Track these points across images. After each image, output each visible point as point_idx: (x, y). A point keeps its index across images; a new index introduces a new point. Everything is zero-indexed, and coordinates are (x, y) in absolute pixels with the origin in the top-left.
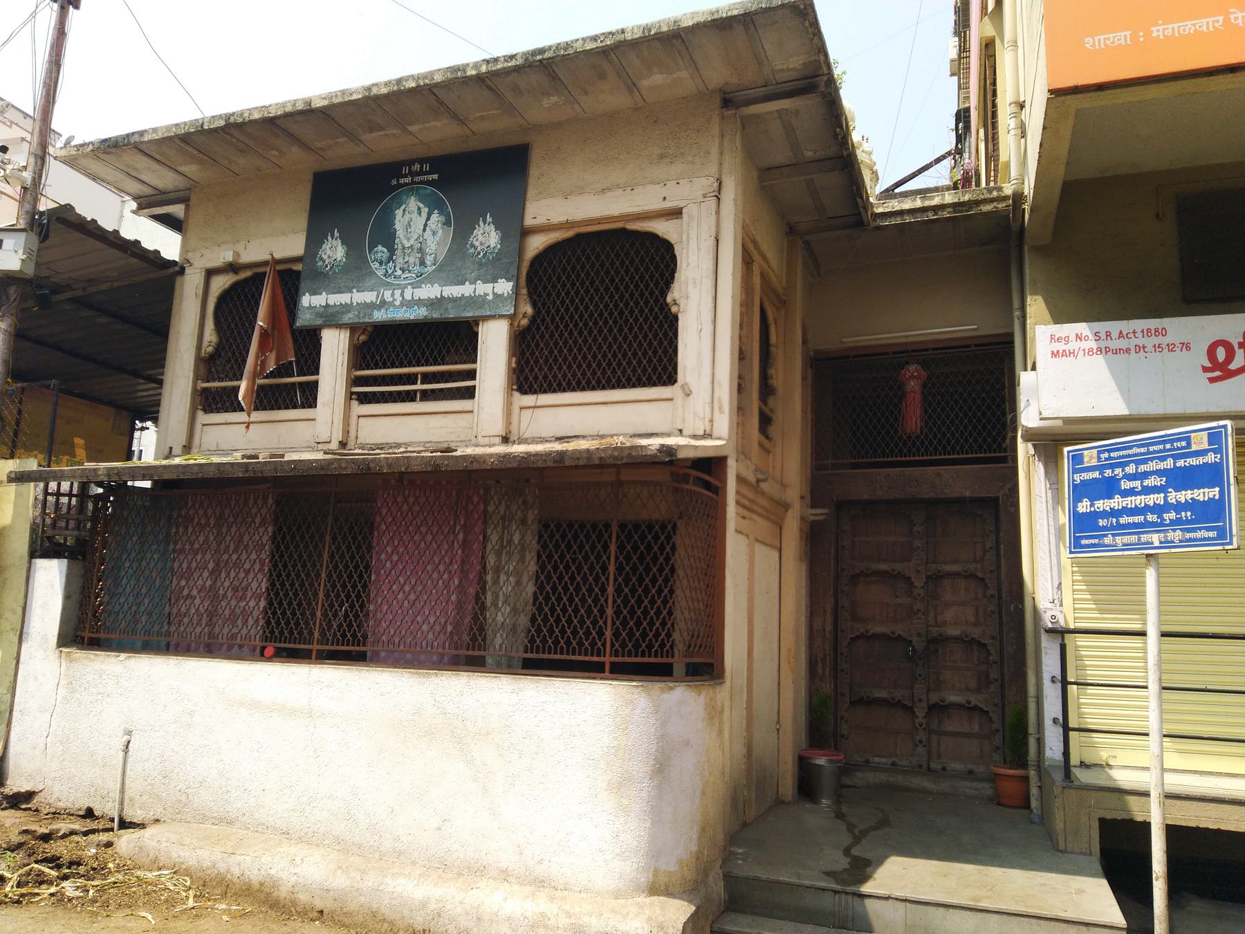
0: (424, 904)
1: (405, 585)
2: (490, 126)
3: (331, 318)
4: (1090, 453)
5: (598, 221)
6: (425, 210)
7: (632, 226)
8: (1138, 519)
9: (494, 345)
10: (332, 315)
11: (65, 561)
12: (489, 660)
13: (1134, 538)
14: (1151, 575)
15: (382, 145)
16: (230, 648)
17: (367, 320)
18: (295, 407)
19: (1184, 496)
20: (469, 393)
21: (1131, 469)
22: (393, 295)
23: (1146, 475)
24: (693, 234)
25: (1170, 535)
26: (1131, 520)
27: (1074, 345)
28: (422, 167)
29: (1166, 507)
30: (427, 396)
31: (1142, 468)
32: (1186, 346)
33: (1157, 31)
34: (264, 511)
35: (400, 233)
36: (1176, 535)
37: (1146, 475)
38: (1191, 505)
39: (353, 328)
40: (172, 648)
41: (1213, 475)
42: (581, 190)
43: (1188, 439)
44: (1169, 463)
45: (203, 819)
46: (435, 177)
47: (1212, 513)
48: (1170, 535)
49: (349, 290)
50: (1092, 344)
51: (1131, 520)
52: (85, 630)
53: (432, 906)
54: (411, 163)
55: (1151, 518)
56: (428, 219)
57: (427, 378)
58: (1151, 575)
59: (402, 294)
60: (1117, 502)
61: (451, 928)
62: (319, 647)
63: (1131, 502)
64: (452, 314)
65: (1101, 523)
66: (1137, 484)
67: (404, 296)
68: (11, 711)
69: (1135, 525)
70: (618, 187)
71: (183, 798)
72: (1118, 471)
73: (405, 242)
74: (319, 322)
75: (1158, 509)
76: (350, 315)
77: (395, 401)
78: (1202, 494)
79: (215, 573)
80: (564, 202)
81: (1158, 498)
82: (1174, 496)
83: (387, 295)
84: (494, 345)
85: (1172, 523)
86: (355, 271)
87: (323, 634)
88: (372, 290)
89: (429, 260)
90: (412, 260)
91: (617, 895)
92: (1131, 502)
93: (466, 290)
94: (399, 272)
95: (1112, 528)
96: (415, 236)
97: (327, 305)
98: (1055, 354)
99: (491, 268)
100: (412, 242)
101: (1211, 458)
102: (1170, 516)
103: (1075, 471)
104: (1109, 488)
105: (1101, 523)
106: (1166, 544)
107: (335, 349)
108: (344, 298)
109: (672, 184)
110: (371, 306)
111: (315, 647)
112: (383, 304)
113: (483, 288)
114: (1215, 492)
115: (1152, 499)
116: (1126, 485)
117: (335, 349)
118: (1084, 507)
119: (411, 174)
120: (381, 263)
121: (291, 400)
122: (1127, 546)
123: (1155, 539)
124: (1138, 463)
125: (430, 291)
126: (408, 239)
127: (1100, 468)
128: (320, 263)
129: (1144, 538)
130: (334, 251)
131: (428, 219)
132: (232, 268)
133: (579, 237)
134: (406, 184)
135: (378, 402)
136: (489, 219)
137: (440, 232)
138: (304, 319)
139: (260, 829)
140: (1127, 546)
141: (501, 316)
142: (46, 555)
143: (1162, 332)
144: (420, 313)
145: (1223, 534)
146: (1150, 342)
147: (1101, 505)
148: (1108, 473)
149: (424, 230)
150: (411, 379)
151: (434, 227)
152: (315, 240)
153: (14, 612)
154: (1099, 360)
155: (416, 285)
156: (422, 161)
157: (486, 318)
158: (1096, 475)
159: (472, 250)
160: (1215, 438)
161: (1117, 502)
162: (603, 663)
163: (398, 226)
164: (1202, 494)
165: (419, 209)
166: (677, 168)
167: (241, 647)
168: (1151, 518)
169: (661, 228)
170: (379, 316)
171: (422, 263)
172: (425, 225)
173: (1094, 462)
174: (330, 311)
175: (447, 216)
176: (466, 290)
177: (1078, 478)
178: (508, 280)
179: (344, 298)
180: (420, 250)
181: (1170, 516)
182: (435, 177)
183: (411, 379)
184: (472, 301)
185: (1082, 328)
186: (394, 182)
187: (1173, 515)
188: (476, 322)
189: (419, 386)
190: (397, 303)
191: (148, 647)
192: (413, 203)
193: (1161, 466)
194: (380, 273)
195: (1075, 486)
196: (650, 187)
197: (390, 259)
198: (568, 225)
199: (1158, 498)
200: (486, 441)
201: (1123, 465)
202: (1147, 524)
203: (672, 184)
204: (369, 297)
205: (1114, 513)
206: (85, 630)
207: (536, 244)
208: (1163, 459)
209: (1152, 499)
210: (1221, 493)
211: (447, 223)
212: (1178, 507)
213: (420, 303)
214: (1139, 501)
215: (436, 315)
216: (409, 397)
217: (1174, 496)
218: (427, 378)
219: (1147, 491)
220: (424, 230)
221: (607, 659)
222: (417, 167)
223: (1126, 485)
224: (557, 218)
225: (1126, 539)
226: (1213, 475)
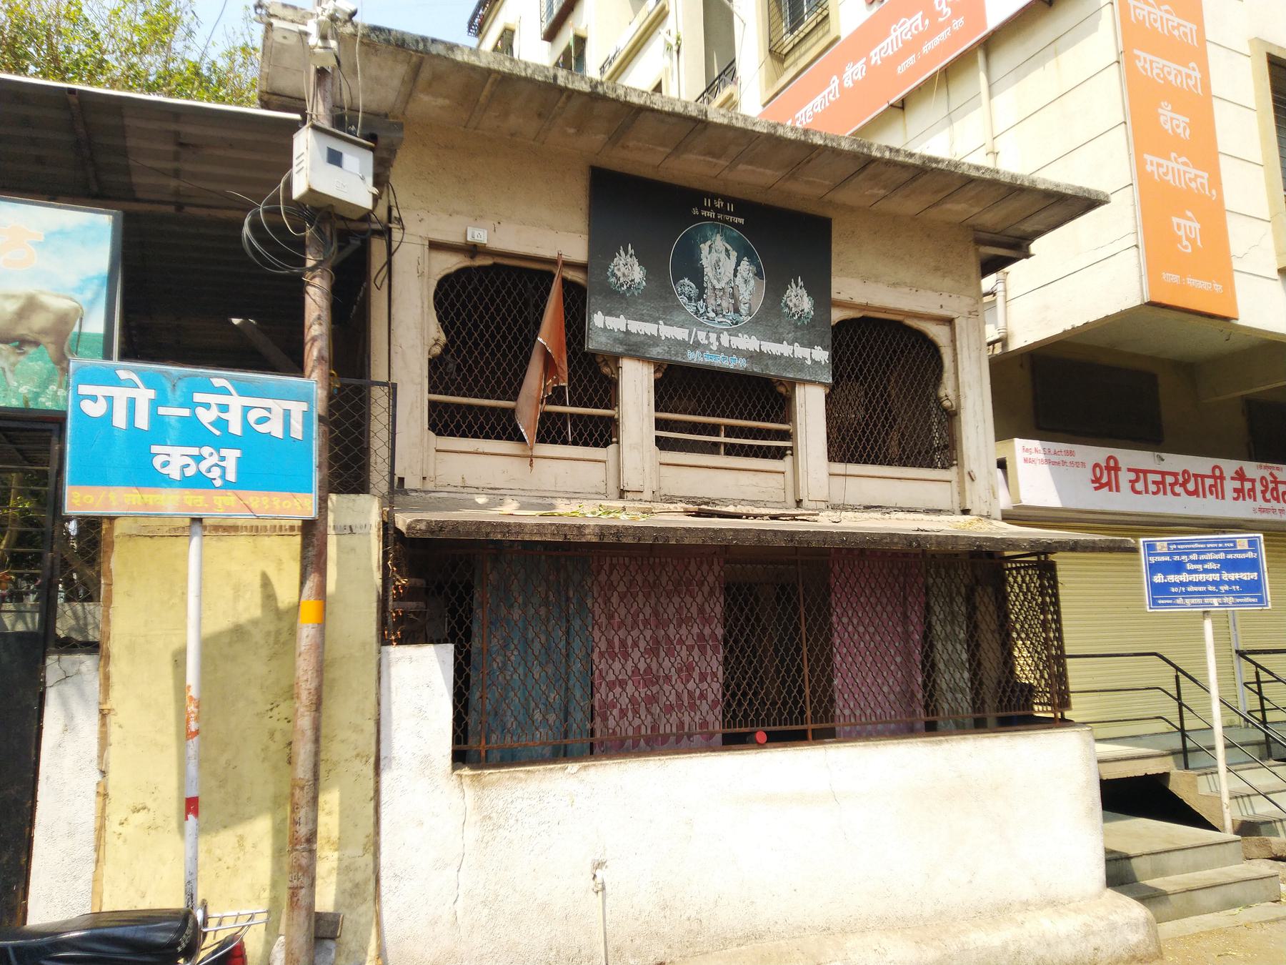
0: (1005, 948)
1: (861, 654)
2: (802, 193)
3: (636, 349)
4: (1162, 543)
5: (885, 310)
6: (734, 254)
7: (909, 322)
8: (1191, 589)
9: (811, 408)
10: (635, 344)
11: (451, 647)
12: (941, 723)
13: (1199, 601)
14: (1208, 625)
15: (690, 168)
16: (678, 740)
17: (679, 359)
18: (565, 442)
19: (1234, 576)
20: (779, 454)
21: (1194, 557)
22: (708, 338)
23: (1205, 562)
24: (965, 345)
25: (1226, 600)
26: (1196, 589)
27: (1034, 456)
28: (725, 206)
29: (1222, 582)
30: (732, 450)
31: (1202, 557)
32: (1083, 464)
33: (1191, 281)
34: (711, 579)
35: (708, 270)
36: (1230, 600)
37: (1205, 562)
38: (1239, 582)
39: (658, 365)
40: (596, 750)
41: (1253, 565)
42: (877, 279)
43: (1234, 542)
44: (1222, 556)
45: (725, 942)
46: (742, 221)
47: (1254, 588)
48: (1226, 600)
49: (655, 321)
50: (1042, 456)
51: (1196, 589)
52: (479, 742)
53: (1012, 948)
54: (714, 197)
55: (1210, 588)
56: (738, 264)
57: (731, 431)
58: (1208, 625)
59: (718, 339)
60: (1184, 577)
61: (1030, 960)
62: (814, 726)
63: (1195, 578)
64: (772, 372)
65: (1173, 590)
66: (1199, 567)
67: (725, 344)
68: (377, 881)
69: (1199, 593)
70: (905, 284)
71: (695, 926)
72: (1184, 558)
73: (715, 282)
74: (619, 349)
75: (1214, 583)
76: (659, 349)
77: (765, 456)
78: (1246, 576)
79: (653, 651)
80: (863, 285)
81: (1216, 577)
82: (1226, 576)
83: (702, 336)
84: (811, 408)
85: (1226, 592)
86: (658, 299)
87: (815, 713)
88: (682, 326)
89: (744, 309)
90: (725, 304)
91: (1099, 896)
92: (1195, 578)
93: (783, 349)
94: (712, 315)
95: (1182, 593)
96: (726, 280)
97: (628, 332)
98: (1026, 460)
99: (807, 332)
100: (722, 285)
101: (1250, 555)
102: (1225, 588)
103: (1150, 555)
104: (1178, 568)
105: (1173, 590)
106: (1222, 604)
107: (636, 385)
108: (648, 328)
109: (945, 295)
110: (683, 344)
111: (810, 726)
112: (697, 345)
113: (801, 352)
114: (1254, 575)
115: (1211, 577)
116: (1190, 566)
117: (636, 385)
118: (1159, 578)
119: (713, 207)
120: (690, 299)
121: (559, 433)
122: (1193, 605)
123: (1215, 601)
124: (1199, 553)
125: (748, 343)
126: (718, 281)
127: (1171, 555)
128: (613, 280)
129: (1207, 601)
130: (628, 269)
131: (738, 264)
132: (473, 250)
133: (864, 319)
134: (708, 219)
135: (757, 456)
136: (801, 283)
137: (752, 282)
138: (595, 343)
139: (796, 934)
140: (1193, 605)
141: (821, 383)
142: (410, 637)
143: (1071, 453)
144: (738, 364)
145: (1261, 600)
146: (1068, 459)
147: (1172, 578)
148: (1176, 558)
149: (735, 276)
150: (714, 430)
151: (745, 275)
152: (602, 248)
153: (358, 729)
154: (1046, 467)
155: (733, 333)
156: (726, 199)
157: (804, 382)
158: (1168, 559)
159: (786, 310)
160: (1252, 543)
161: (1184, 577)
162: (805, 731)
163: (704, 262)
164: (1246, 576)
165: (727, 250)
166: (948, 282)
167: (690, 736)
168: (1210, 588)
169: (938, 333)
170: (694, 357)
171: (737, 311)
172: (736, 271)
173: (1165, 550)
174: (633, 339)
175: (758, 266)
176: (783, 349)
177: (1153, 560)
178: (824, 349)
179: (648, 328)
180: (733, 296)
181: (1225, 588)
182: (742, 221)
183: (714, 430)
184: (791, 362)
185: (1036, 444)
186: (695, 212)
187: (1227, 588)
188: (792, 384)
189: (722, 439)
190: (714, 348)
191: (561, 753)
192: (719, 242)
193: (1217, 557)
194: (690, 309)
195: (1151, 565)
196: (929, 293)
197: (700, 297)
198: (866, 307)
199: (1216, 577)
200: (813, 505)
201: (1188, 554)
202: (1208, 592)
203: (945, 295)
204: (680, 334)
205: (1182, 584)
206: (479, 742)
207: (837, 315)
208: (1217, 552)
209: (1211, 577)
210: (1259, 576)
211: (758, 274)
212: (1230, 583)
213: (738, 352)
214: (1203, 577)
215: (757, 369)
216: (713, 449)
217: (1226, 576)
218: (731, 431)
219: (1206, 571)
220: (735, 276)
221: (810, 726)
222: (719, 204)
223: (1190, 566)
224: (860, 299)
225: (1193, 601)
226: (1253, 565)
